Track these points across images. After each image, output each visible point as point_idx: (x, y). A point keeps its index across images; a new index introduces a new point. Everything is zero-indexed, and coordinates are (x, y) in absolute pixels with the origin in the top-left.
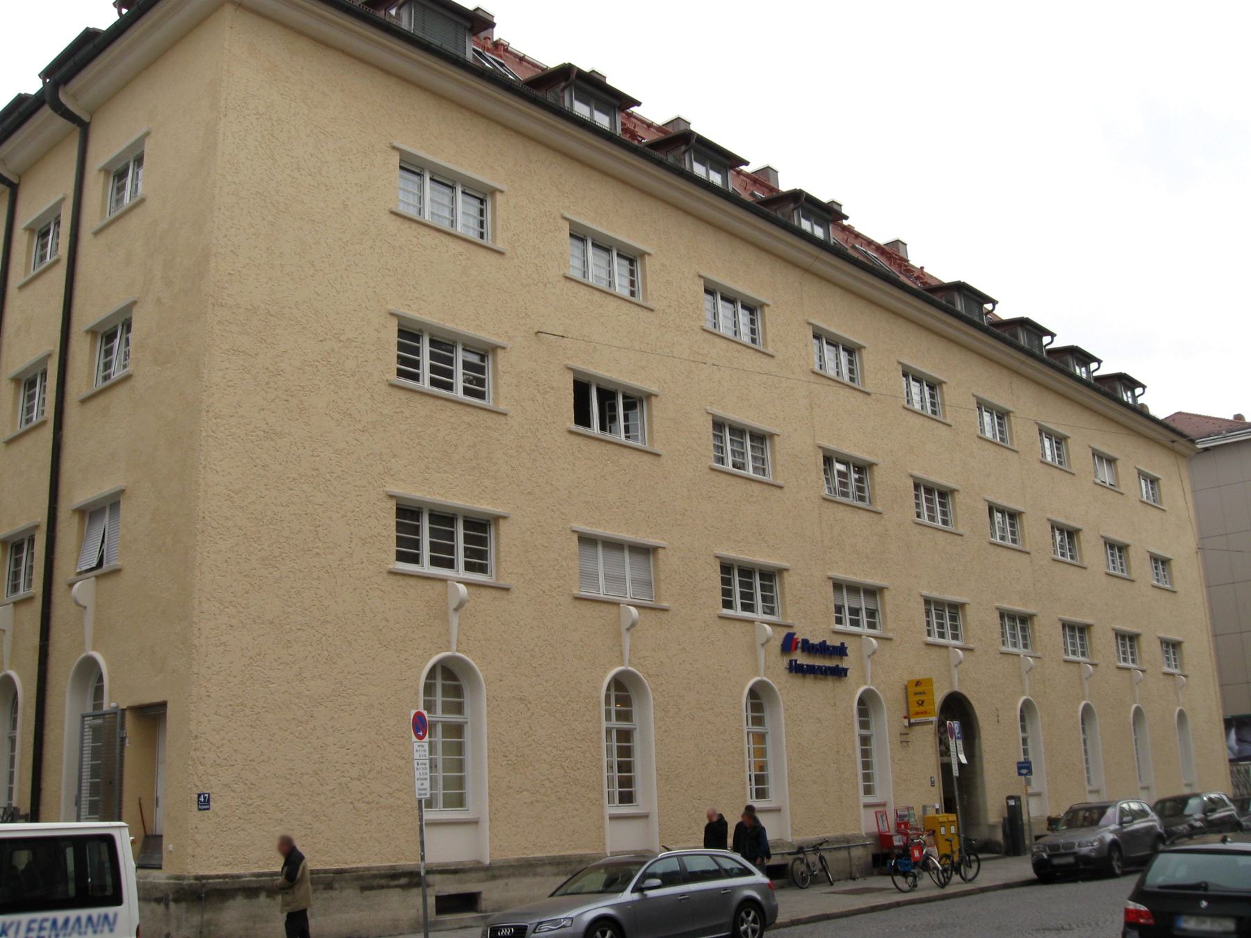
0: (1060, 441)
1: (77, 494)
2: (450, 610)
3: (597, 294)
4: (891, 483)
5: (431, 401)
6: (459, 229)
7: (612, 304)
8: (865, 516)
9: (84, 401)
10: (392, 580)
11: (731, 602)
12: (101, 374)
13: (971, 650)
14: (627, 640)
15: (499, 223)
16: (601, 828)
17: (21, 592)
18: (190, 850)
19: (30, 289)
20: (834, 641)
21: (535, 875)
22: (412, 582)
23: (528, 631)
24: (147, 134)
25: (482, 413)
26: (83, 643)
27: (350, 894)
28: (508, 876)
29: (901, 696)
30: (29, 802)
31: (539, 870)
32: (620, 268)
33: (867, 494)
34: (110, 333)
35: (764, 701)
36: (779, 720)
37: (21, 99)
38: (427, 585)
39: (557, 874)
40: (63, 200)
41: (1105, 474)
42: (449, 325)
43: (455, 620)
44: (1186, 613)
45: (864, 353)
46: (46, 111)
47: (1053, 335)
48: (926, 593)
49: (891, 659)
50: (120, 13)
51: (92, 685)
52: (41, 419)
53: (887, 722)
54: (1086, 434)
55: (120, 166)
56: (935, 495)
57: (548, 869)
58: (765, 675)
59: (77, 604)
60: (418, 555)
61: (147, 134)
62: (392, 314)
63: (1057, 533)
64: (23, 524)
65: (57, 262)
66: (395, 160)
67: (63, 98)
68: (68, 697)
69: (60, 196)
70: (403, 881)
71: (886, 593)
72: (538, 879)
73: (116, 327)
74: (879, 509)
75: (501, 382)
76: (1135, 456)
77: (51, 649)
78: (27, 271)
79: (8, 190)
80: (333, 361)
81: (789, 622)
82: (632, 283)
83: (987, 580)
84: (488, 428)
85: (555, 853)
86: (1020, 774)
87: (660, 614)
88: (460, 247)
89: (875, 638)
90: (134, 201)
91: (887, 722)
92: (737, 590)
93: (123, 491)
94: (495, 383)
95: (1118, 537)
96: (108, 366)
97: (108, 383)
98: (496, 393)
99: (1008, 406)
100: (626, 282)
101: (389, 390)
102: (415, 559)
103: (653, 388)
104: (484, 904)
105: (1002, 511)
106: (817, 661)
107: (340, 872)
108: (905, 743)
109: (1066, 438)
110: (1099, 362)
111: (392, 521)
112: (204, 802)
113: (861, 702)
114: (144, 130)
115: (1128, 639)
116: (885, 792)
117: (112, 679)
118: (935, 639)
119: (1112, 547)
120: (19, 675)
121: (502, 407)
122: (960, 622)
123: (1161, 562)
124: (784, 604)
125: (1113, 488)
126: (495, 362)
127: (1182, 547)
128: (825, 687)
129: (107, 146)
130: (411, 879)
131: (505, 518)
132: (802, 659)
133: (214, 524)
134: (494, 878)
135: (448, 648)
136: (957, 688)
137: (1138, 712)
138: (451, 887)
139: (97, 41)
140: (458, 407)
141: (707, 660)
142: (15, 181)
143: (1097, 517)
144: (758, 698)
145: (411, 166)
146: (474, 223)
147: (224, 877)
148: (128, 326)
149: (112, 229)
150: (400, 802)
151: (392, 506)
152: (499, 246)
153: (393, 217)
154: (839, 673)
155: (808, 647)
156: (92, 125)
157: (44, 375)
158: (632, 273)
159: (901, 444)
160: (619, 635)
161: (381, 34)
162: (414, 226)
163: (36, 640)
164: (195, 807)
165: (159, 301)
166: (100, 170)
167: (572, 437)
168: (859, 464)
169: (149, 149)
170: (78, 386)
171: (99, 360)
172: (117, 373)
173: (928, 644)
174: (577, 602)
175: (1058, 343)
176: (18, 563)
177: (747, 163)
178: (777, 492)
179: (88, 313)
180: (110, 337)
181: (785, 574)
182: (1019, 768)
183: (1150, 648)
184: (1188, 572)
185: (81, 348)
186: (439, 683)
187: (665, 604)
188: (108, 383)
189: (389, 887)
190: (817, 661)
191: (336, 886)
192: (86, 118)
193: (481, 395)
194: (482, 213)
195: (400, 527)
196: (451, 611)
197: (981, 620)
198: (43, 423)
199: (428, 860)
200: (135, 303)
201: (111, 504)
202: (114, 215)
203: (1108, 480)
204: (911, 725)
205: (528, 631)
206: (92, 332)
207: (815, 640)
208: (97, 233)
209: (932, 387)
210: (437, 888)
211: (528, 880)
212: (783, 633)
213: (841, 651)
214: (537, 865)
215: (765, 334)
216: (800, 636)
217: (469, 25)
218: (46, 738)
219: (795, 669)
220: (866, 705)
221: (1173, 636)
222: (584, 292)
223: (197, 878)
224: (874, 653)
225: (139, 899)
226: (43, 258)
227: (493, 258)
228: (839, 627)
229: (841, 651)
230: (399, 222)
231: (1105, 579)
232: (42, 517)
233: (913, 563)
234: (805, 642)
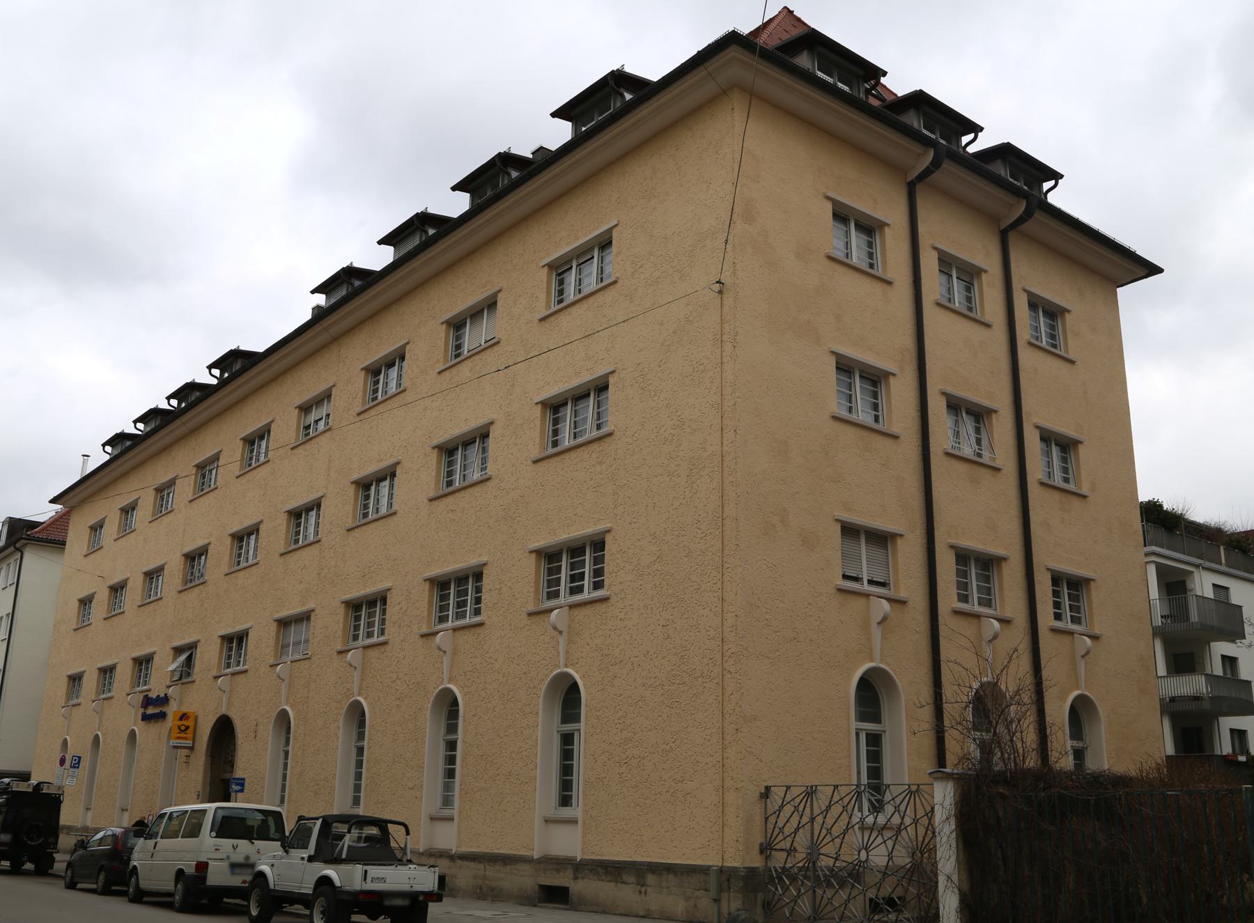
6: (855, 260)
11: (967, 596)
13: (903, 603)
14: (1082, 665)
32: (857, 240)
33: (1071, 476)
58: (882, 661)
62: (1037, 427)
63: (1055, 451)
82: (871, 255)
89: (888, 600)
92: (1066, 602)
109: (1063, 311)
113: (1073, 710)
122: (1084, 604)
158: (870, 245)
175: (983, 142)
177: (975, 129)
196: (874, 625)
224: (1087, 653)
228: (1058, 624)
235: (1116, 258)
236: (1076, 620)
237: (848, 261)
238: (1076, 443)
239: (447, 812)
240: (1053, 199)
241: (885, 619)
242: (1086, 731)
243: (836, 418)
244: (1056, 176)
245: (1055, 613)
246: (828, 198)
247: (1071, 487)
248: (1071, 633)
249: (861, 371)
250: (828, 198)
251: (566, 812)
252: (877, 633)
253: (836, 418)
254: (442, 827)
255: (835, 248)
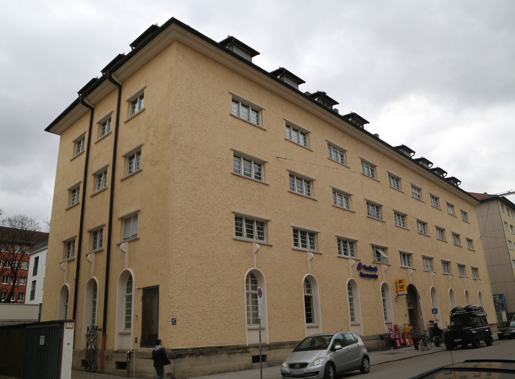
0: (436, 199)
1: (121, 212)
2: (250, 255)
3: (295, 145)
4: (387, 212)
5: (245, 180)
6: (252, 122)
7: (300, 149)
8: (380, 223)
9: (122, 180)
10: (234, 242)
12: (128, 171)
14: (309, 264)
15: (264, 120)
16: (304, 331)
17: (97, 249)
18: (169, 340)
19: (99, 143)
20: (373, 266)
21: (284, 348)
22: (241, 243)
23: (279, 261)
24: (145, 87)
25: (261, 184)
26: (124, 265)
27: (224, 356)
28: (276, 349)
29: (394, 285)
30: (102, 324)
31: (285, 346)
32: (301, 137)
33: (380, 216)
34: (133, 156)
35: (352, 287)
36: (358, 294)
37: (94, 80)
38: (246, 244)
39: (291, 348)
40: (86, 132)
41: (451, 211)
42: (250, 154)
43: (255, 256)
44: (478, 258)
45: (377, 168)
46: (80, 105)
47: (432, 164)
48: (400, 250)
49: (391, 272)
50: (132, 48)
51: (126, 281)
52: (77, 202)
53: (391, 294)
54: (444, 198)
55: (134, 99)
56: (401, 216)
57: (289, 346)
59: (122, 251)
60: (242, 234)
61: (145, 87)
62: (232, 149)
63: (304, 183)
64: (98, 224)
65: (84, 152)
66: (230, 97)
67: (85, 101)
68: (118, 285)
69: (84, 131)
70: (241, 351)
71: (388, 250)
72: (285, 350)
73: (134, 154)
74: (384, 220)
75: (266, 174)
76: (459, 206)
77: (110, 268)
78: (74, 154)
79: (90, 110)
80: (213, 165)
81: (359, 259)
83: (418, 247)
84: (263, 190)
85: (290, 340)
86: (433, 313)
87: (319, 256)
88: (252, 127)
90: (108, 133)
91: (391, 294)
92: (308, 241)
93: (139, 211)
94: (265, 174)
95: (457, 232)
96: (130, 168)
97: (131, 174)
98: (265, 178)
99: (421, 187)
100: (303, 142)
101: (231, 175)
102: (241, 235)
103: (314, 178)
104: (268, 359)
105: (420, 223)
106: (368, 273)
107: (221, 347)
108: (397, 302)
110: (447, 173)
111: (234, 221)
112: (174, 322)
114: (144, 86)
115: (461, 267)
116: (392, 319)
117: (136, 278)
118: (404, 266)
119: (454, 235)
120: (98, 279)
121: (267, 182)
123: (470, 241)
124: (357, 253)
125: (453, 215)
126: (264, 167)
127: (475, 236)
128: (372, 281)
129: (128, 93)
130: (244, 349)
131: (270, 221)
132: (364, 272)
133: (176, 221)
134: (270, 349)
135: (253, 267)
136: (411, 283)
137: (466, 292)
138: (257, 353)
139: (123, 58)
140: (254, 182)
141: (334, 272)
142: (93, 107)
143: (452, 225)
144: (351, 285)
145: (236, 100)
146: (255, 119)
147: (181, 349)
148: (139, 153)
149: (132, 120)
150: (239, 322)
151: (234, 215)
152: (264, 127)
153: (231, 116)
154: (375, 277)
155: (366, 268)
156: (123, 87)
157: (79, 188)
159: (391, 200)
160: (307, 263)
161: (226, 54)
162: (237, 120)
163: (105, 265)
164: (171, 323)
165: (152, 143)
166: (97, 123)
167: (289, 194)
168: (377, 206)
169: (146, 92)
170: (90, 191)
171: (127, 165)
172: (134, 170)
173: (402, 267)
174: (293, 251)
175: (434, 167)
176: (95, 239)
178: (353, 214)
179: (124, 149)
180: (100, 176)
181: (357, 242)
182: (433, 311)
183: (468, 270)
184: (478, 244)
185: (91, 179)
186: (250, 279)
187: (321, 252)
188: (131, 174)
189: (237, 353)
190: (368, 273)
191: (219, 352)
192: (121, 84)
193: (260, 179)
194: (257, 116)
195: (236, 224)
197: (417, 260)
198: (79, 204)
199: (262, 342)
200: (142, 145)
201: (135, 216)
202: (132, 116)
203: (452, 213)
204: (398, 295)
205: (279, 261)
206: (125, 156)
207: (368, 266)
208: (96, 143)
209: (397, 180)
210: (252, 353)
211: (282, 350)
212: (358, 262)
213: (375, 269)
214: (285, 345)
215: (347, 161)
216: (363, 264)
217: (251, 53)
218: (108, 301)
219: (362, 275)
220: (385, 287)
221: (475, 266)
222: (291, 144)
223: (173, 350)
224: (312, 259)
225: (73, 368)
226: (79, 151)
227: (262, 131)
229: (375, 269)
230: (233, 118)
231: (453, 246)
232: (106, 222)
233: (396, 240)
234: (365, 266)
235: (189, 34)
236: (409, 265)
237: (249, 122)
238: (459, 235)
239: (127, 331)
240: (459, 186)
241: (258, 251)
242: (312, 289)
243: (289, 192)
244: (367, 122)
245: (295, 244)
246: (230, 93)
247: (405, 228)
248: (407, 268)
249: (254, 161)
250: (230, 93)
251: (127, 331)
252: (309, 264)
253: (289, 192)
254: (126, 339)
255: (244, 117)
